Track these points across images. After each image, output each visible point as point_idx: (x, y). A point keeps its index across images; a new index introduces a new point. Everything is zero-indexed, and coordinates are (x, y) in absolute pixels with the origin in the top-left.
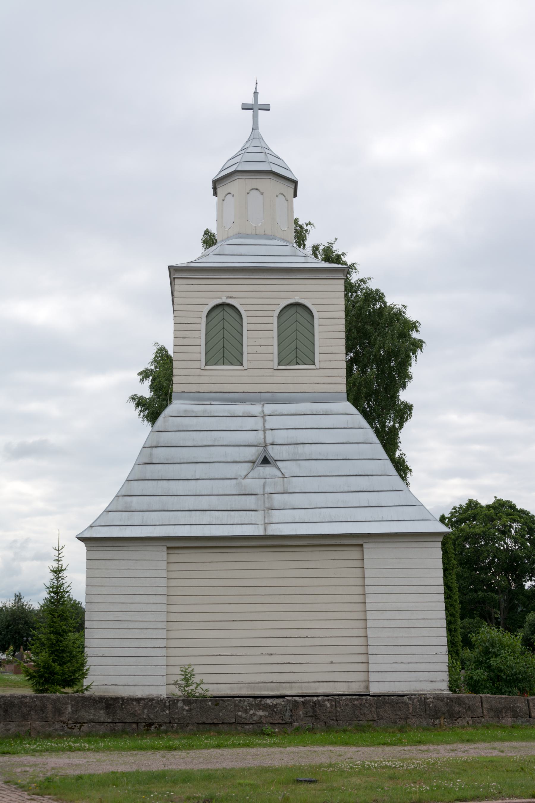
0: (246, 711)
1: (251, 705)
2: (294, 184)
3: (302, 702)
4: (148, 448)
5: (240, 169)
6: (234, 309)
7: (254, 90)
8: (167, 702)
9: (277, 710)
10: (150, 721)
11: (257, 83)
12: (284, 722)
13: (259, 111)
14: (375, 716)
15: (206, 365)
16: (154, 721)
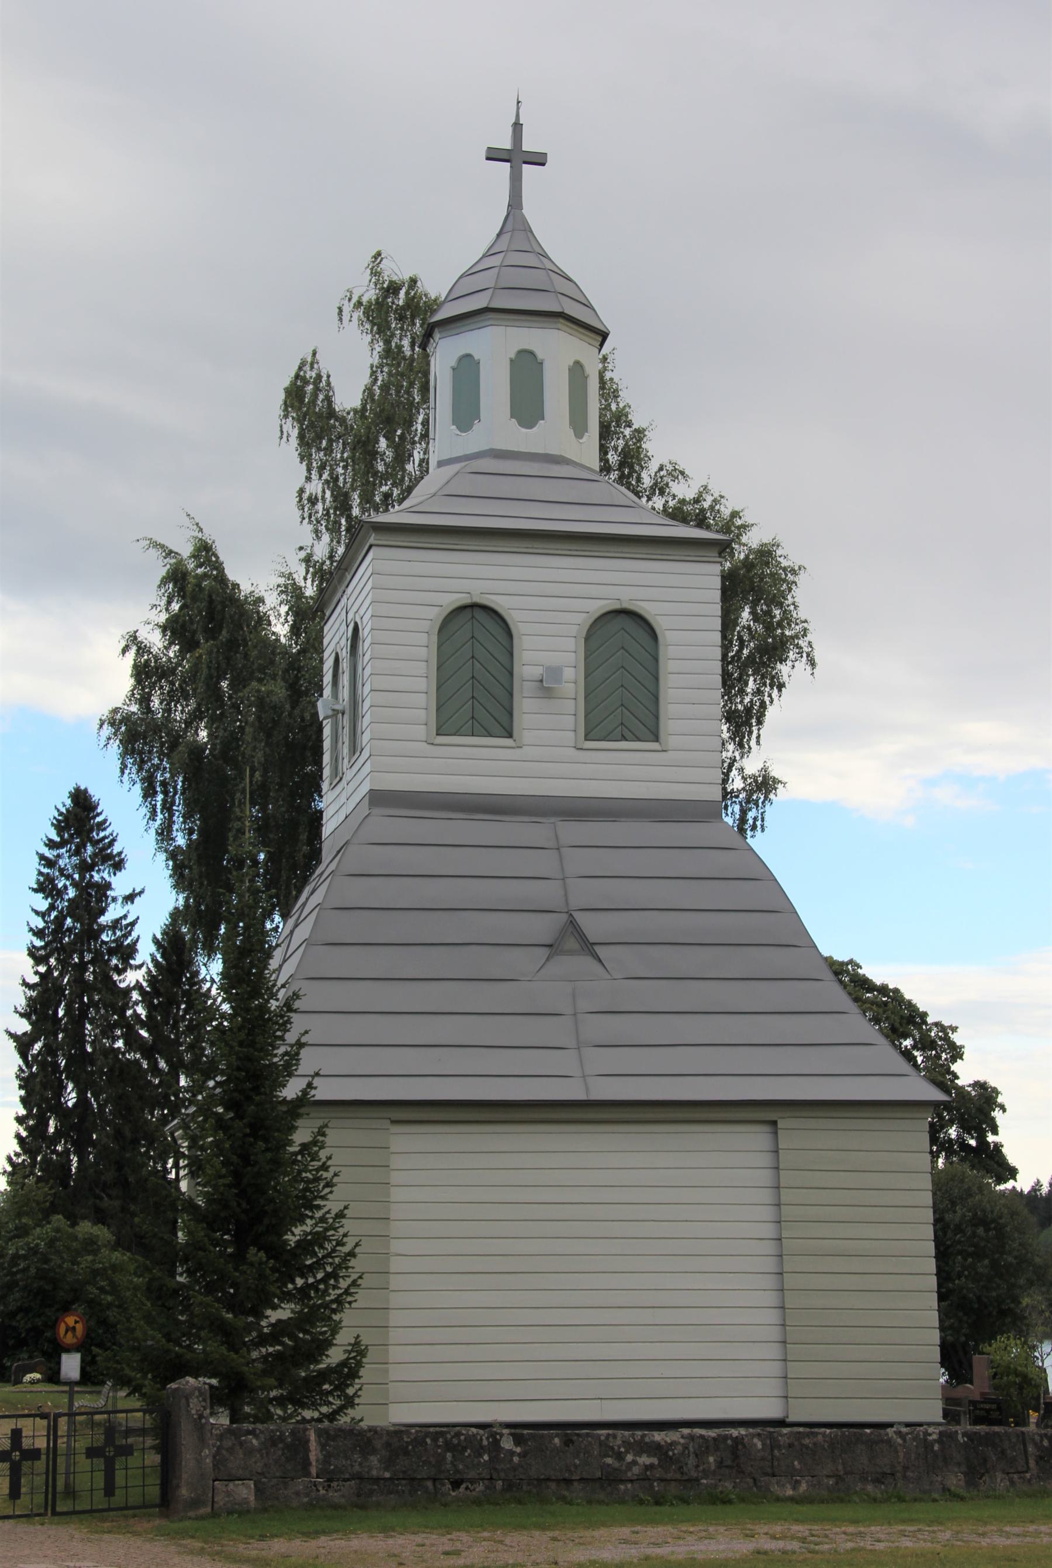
0: (620, 1457)
1: (629, 1446)
2: (600, 339)
3: (714, 1439)
4: (334, 911)
5: (496, 304)
6: (497, 618)
7: (513, 120)
8: (484, 1438)
9: (674, 1454)
10: (458, 1476)
11: (518, 102)
12: (686, 1478)
13: (524, 166)
14: (840, 1468)
15: (437, 735)
16: (465, 1476)
